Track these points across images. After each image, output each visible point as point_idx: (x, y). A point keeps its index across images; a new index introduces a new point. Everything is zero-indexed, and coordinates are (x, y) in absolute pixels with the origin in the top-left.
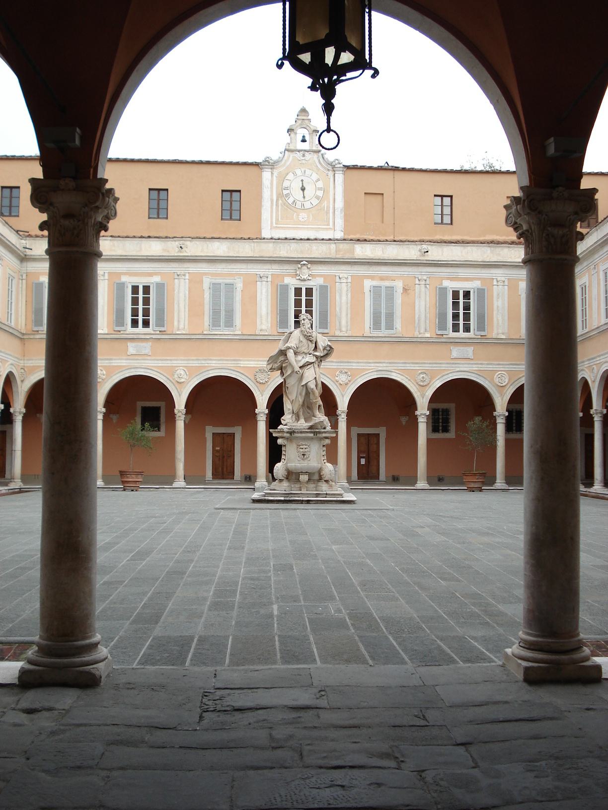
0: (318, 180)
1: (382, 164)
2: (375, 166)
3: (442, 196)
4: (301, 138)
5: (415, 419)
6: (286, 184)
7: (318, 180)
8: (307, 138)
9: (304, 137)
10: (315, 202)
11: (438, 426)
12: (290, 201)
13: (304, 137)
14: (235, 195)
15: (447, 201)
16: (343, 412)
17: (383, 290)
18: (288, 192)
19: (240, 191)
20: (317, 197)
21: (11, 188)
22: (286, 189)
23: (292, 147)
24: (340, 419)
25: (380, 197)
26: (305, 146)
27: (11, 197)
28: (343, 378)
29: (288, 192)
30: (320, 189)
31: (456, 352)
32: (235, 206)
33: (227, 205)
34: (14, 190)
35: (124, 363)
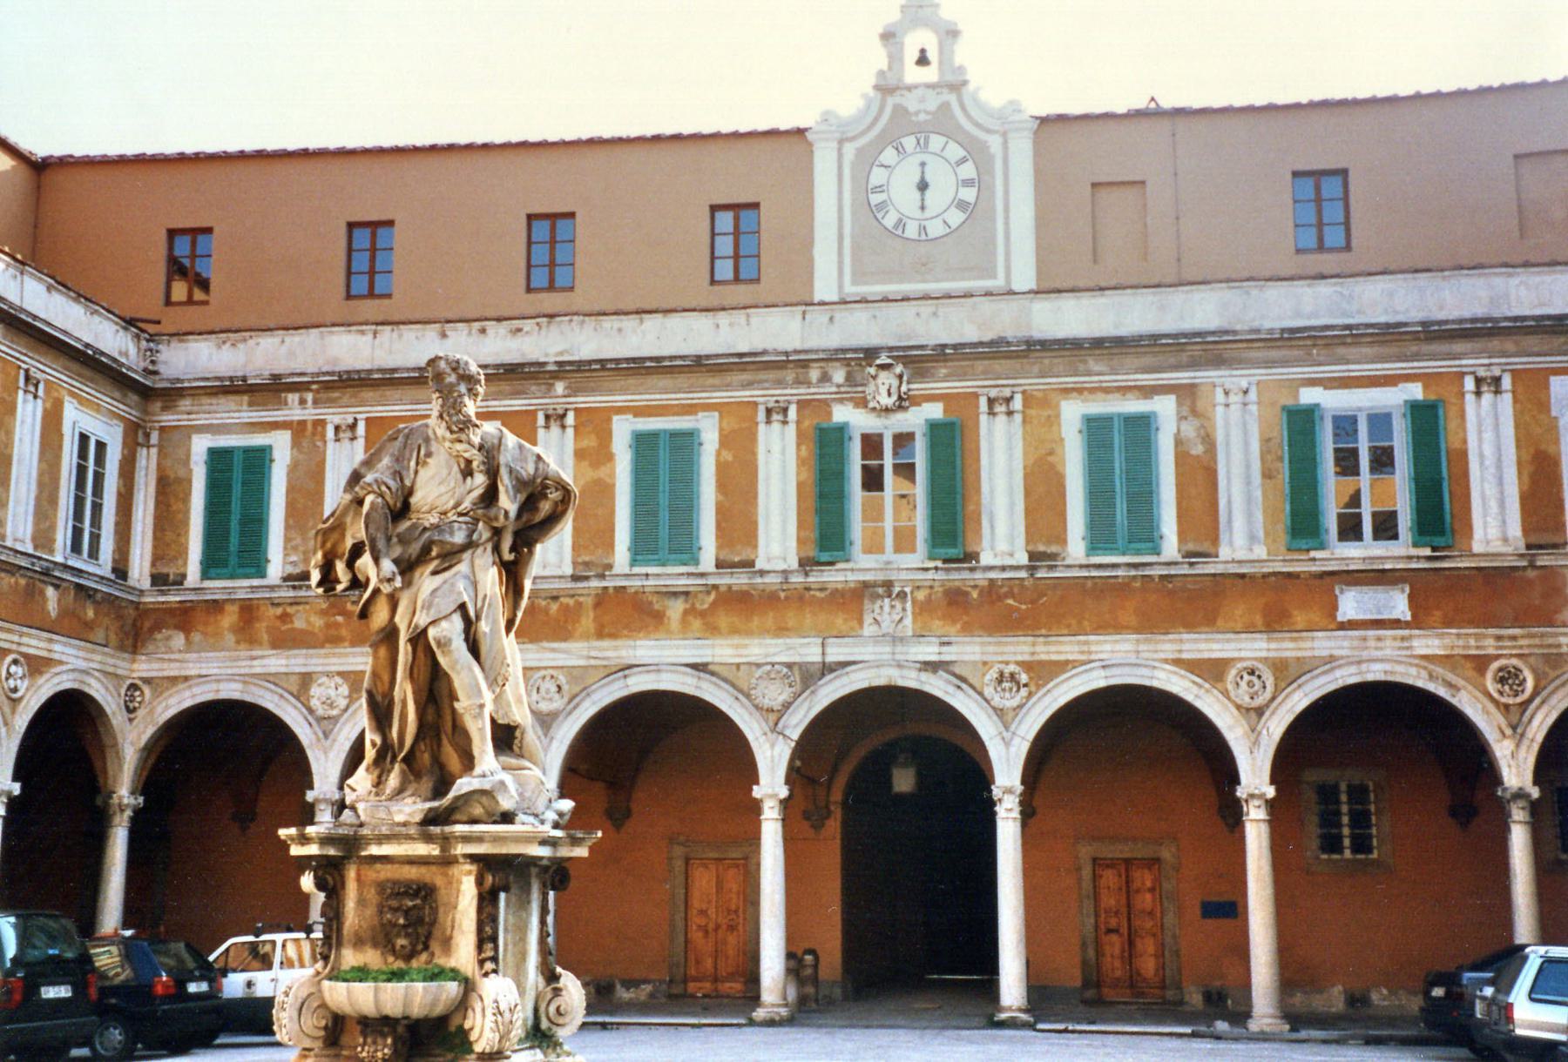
0: (963, 161)
1: (1141, 103)
2: (1121, 110)
3: (1318, 175)
4: (916, 55)
5: (756, 807)
6: (878, 176)
7: (963, 161)
8: (932, 55)
9: (923, 51)
10: (956, 218)
11: (1340, 837)
12: (890, 221)
13: (923, 51)
14: (745, 215)
15: (1331, 187)
16: (1009, 791)
17: (238, 461)
18: (883, 197)
19: (1343, 173)
20: (962, 205)
21: (553, 217)
22: (879, 189)
23: (892, 82)
24: (1000, 810)
25: (1130, 194)
26: (930, 74)
27: (553, 242)
28: (775, 694)
29: (883, 197)
30: (968, 183)
31: (1351, 604)
32: (1333, 212)
33: (541, 254)
34: (560, 223)
35: (1322, 644)
